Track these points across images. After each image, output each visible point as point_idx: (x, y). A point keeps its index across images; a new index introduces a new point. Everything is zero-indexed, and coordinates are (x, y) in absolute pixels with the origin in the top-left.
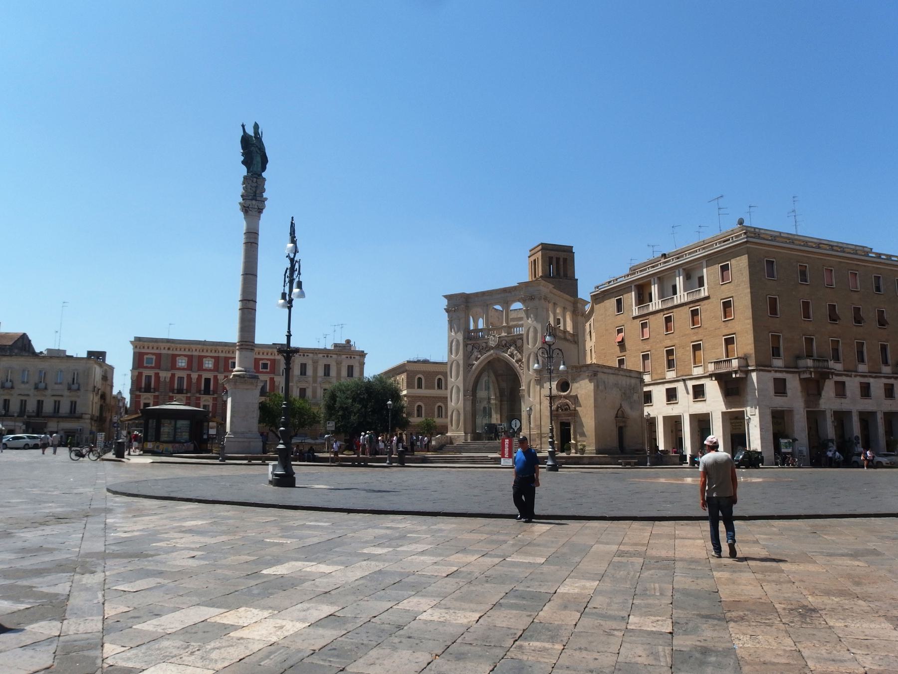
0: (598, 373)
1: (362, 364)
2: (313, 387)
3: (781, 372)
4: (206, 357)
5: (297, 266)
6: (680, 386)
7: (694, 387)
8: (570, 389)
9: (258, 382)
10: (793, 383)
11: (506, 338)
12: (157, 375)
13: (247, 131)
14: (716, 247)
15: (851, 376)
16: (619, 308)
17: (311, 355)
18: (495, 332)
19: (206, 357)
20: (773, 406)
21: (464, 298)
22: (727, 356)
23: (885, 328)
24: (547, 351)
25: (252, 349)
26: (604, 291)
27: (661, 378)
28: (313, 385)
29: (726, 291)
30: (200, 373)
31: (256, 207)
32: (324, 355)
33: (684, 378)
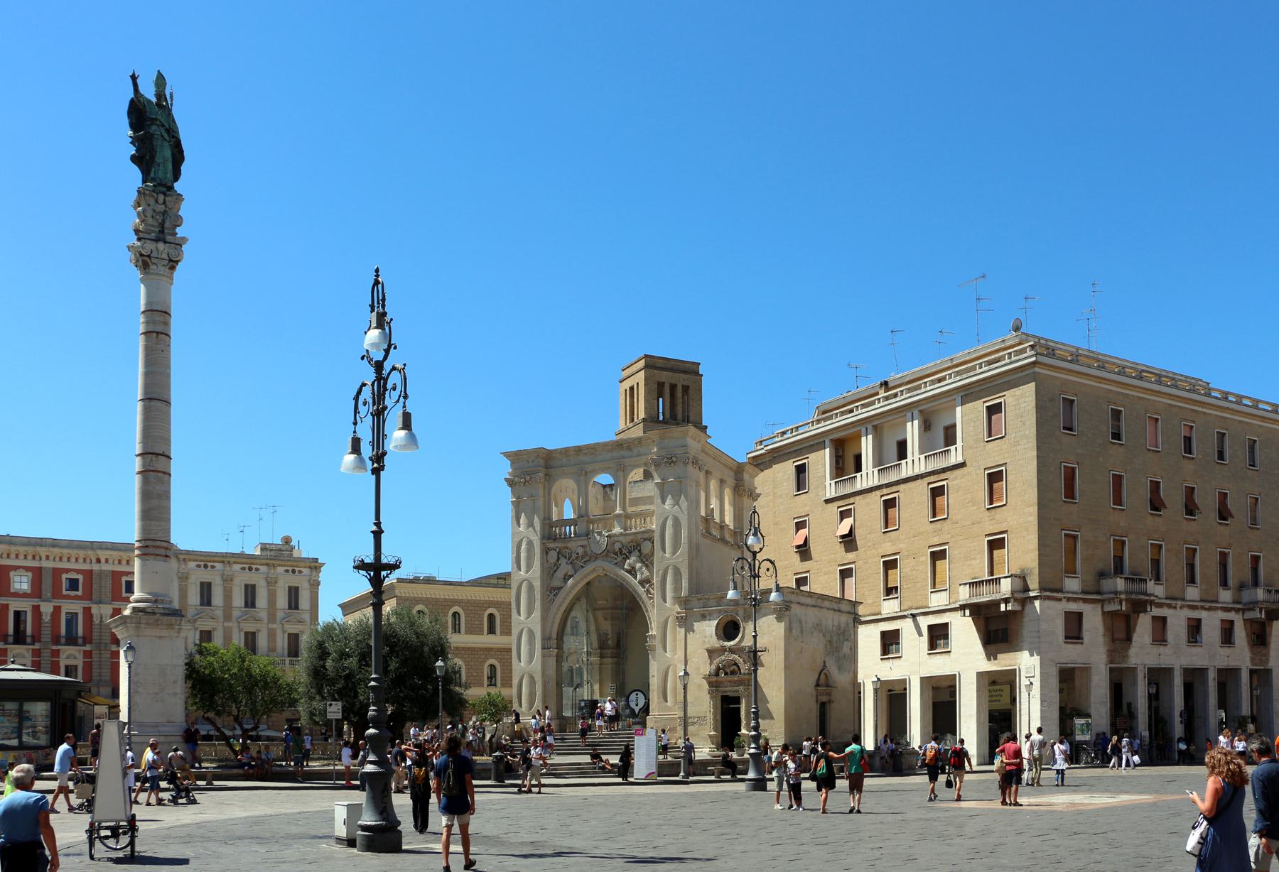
0: (792, 605)
1: (315, 585)
2: (268, 629)
3: (1075, 600)
4: (16, 568)
5: (395, 379)
6: (906, 627)
7: (931, 628)
8: (741, 632)
9: (183, 623)
10: (1093, 620)
11: (621, 538)
12: (87, 611)
13: (142, 90)
14: (981, 370)
15: (1175, 608)
16: (801, 484)
17: (219, 566)
18: (600, 525)
19: (16, 568)
20: (1061, 661)
21: (543, 458)
22: (992, 573)
23: (1227, 524)
24: (750, 565)
25: (167, 556)
26: (773, 449)
27: (873, 612)
28: (270, 626)
29: (994, 455)
30: (57, 603)
31: (165, 256)
32: (200, 563)
33: (914, 612)
